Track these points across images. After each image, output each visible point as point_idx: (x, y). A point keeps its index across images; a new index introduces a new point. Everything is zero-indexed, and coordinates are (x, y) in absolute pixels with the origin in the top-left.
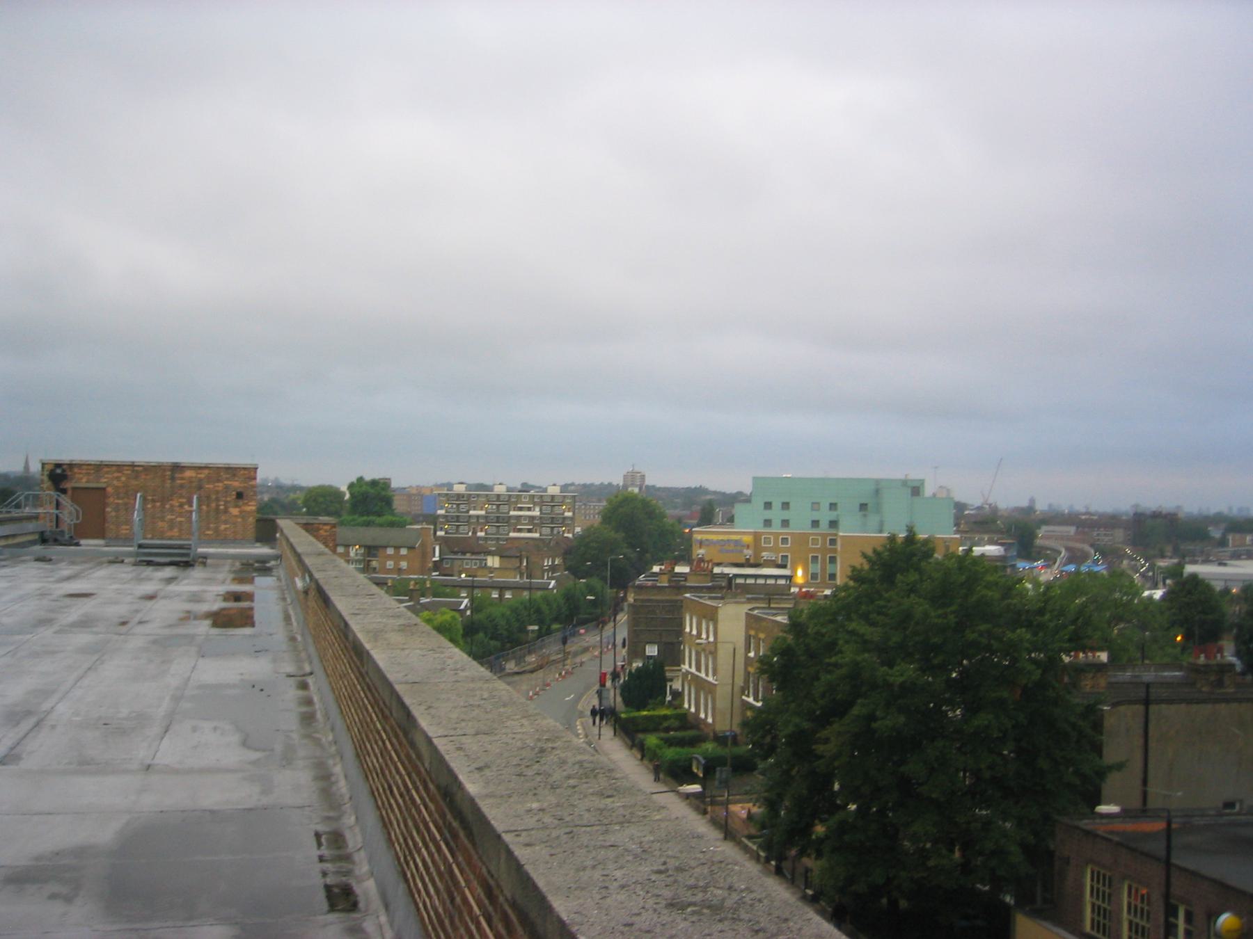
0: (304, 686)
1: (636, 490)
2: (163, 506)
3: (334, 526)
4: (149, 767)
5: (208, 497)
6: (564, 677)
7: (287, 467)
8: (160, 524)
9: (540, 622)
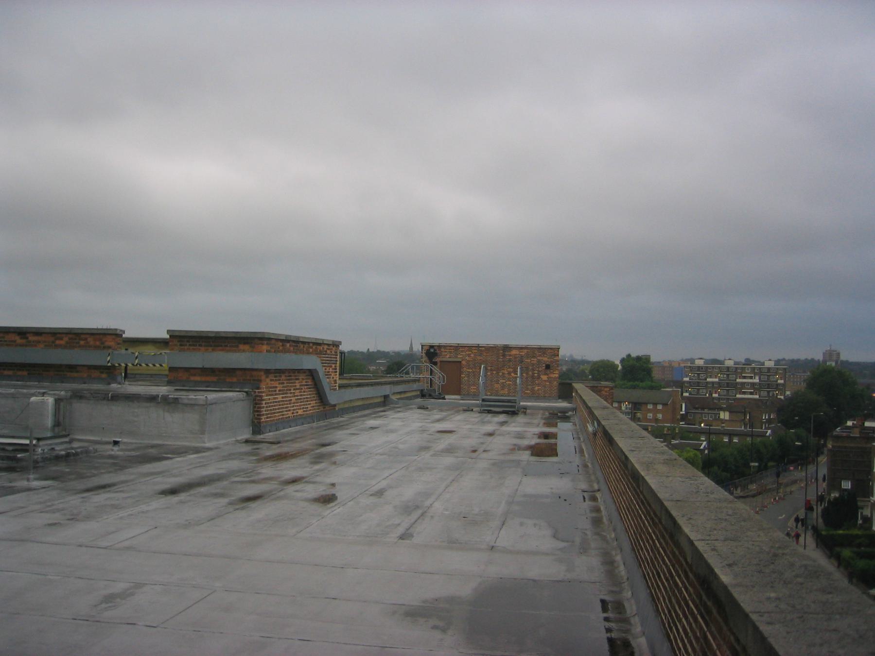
0: (594, 499)
1: (833, 364)
2: (498, 373)
3: (612, 388)
4: (493, 547)
5: (527, 368)
6: (777, 502)
7: (580, 347)
8: (496, 386)
9: (760, 460)
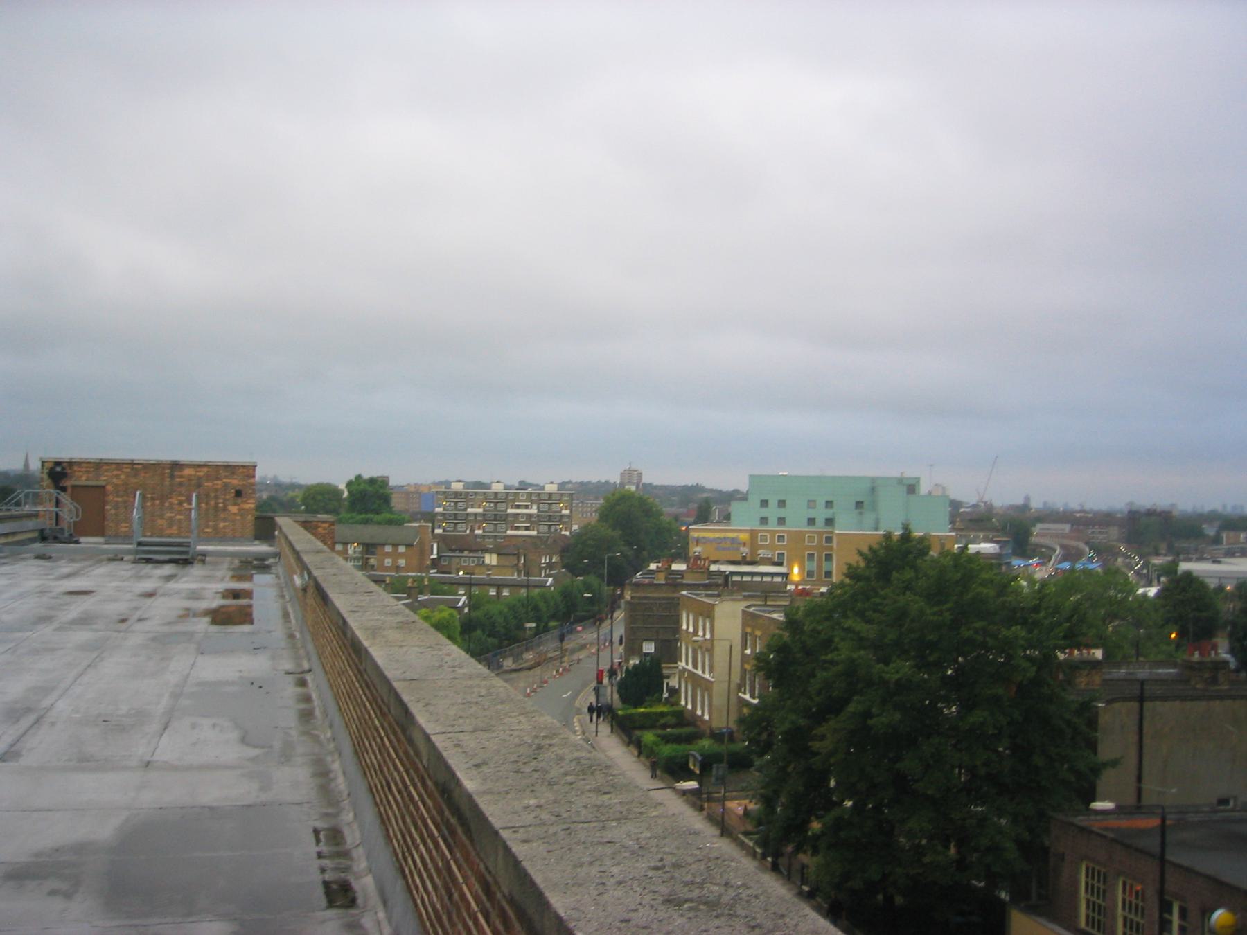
0: (302, 683)
1: (633, 488)
2: (162, 504)
3: (332, 524)
4: (148, 763)
5: (207, 495)
6: (561, 674)
7: (285, 465)
8: (160, 522)
9: (538, 619)
